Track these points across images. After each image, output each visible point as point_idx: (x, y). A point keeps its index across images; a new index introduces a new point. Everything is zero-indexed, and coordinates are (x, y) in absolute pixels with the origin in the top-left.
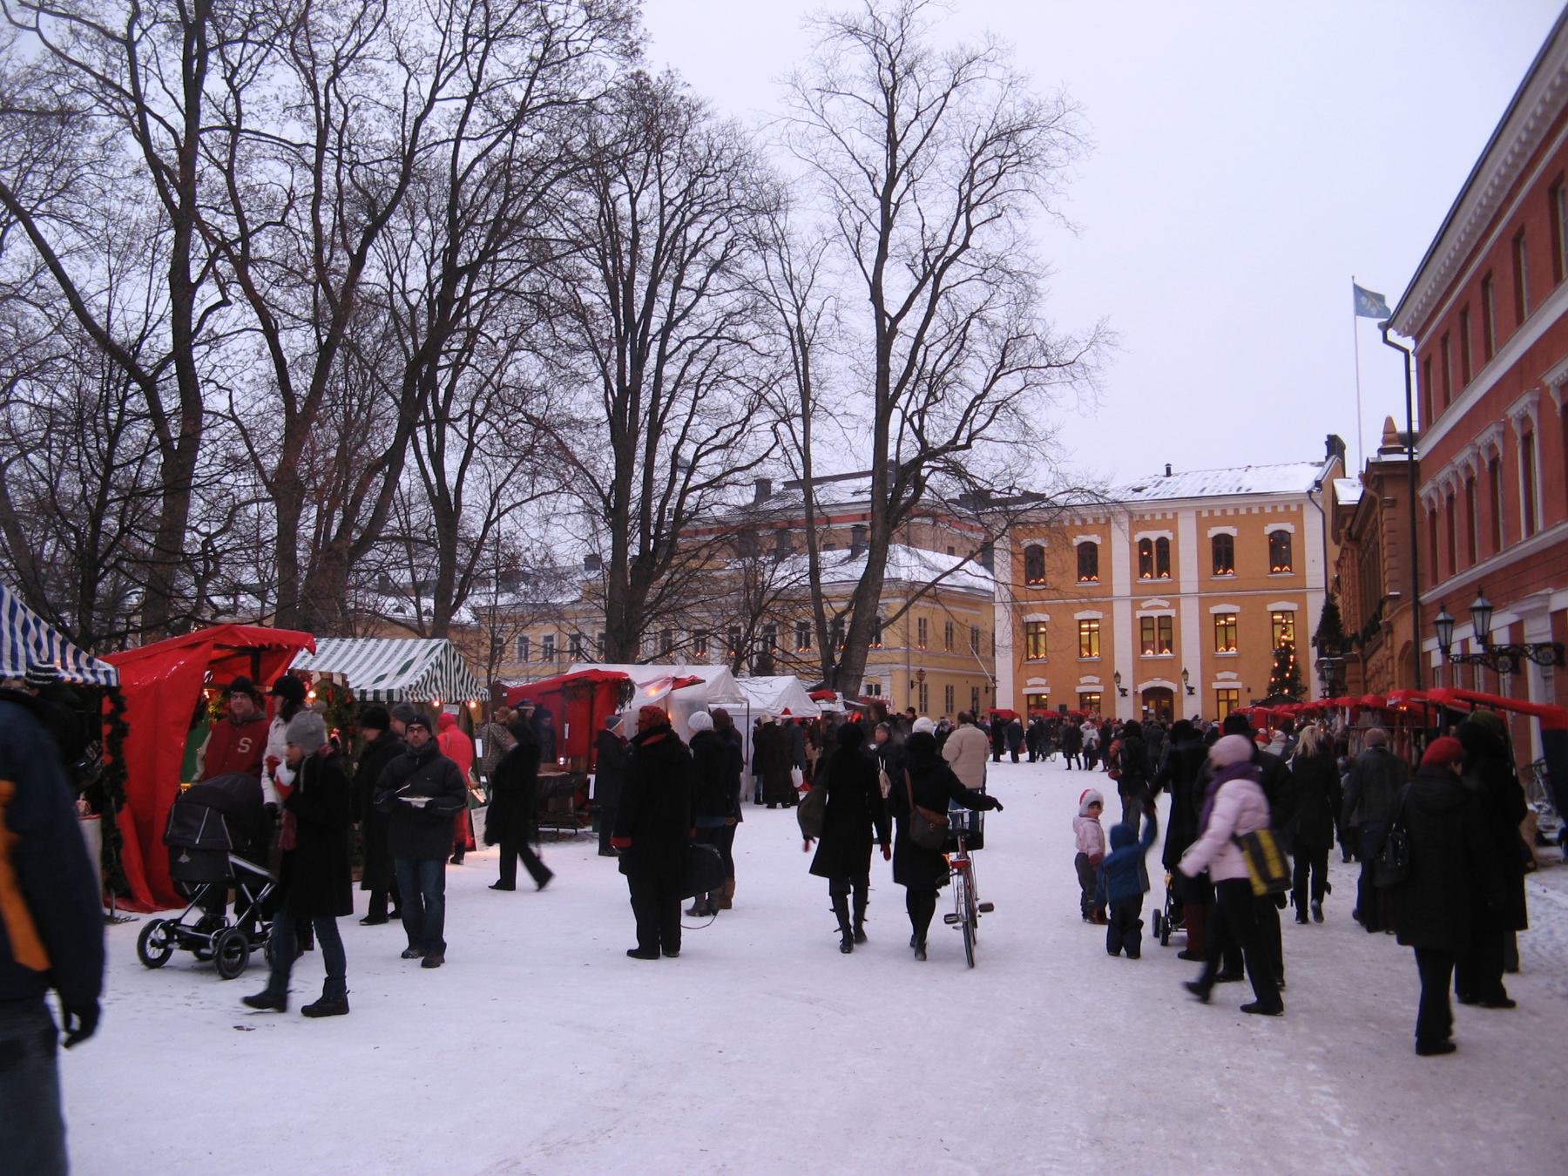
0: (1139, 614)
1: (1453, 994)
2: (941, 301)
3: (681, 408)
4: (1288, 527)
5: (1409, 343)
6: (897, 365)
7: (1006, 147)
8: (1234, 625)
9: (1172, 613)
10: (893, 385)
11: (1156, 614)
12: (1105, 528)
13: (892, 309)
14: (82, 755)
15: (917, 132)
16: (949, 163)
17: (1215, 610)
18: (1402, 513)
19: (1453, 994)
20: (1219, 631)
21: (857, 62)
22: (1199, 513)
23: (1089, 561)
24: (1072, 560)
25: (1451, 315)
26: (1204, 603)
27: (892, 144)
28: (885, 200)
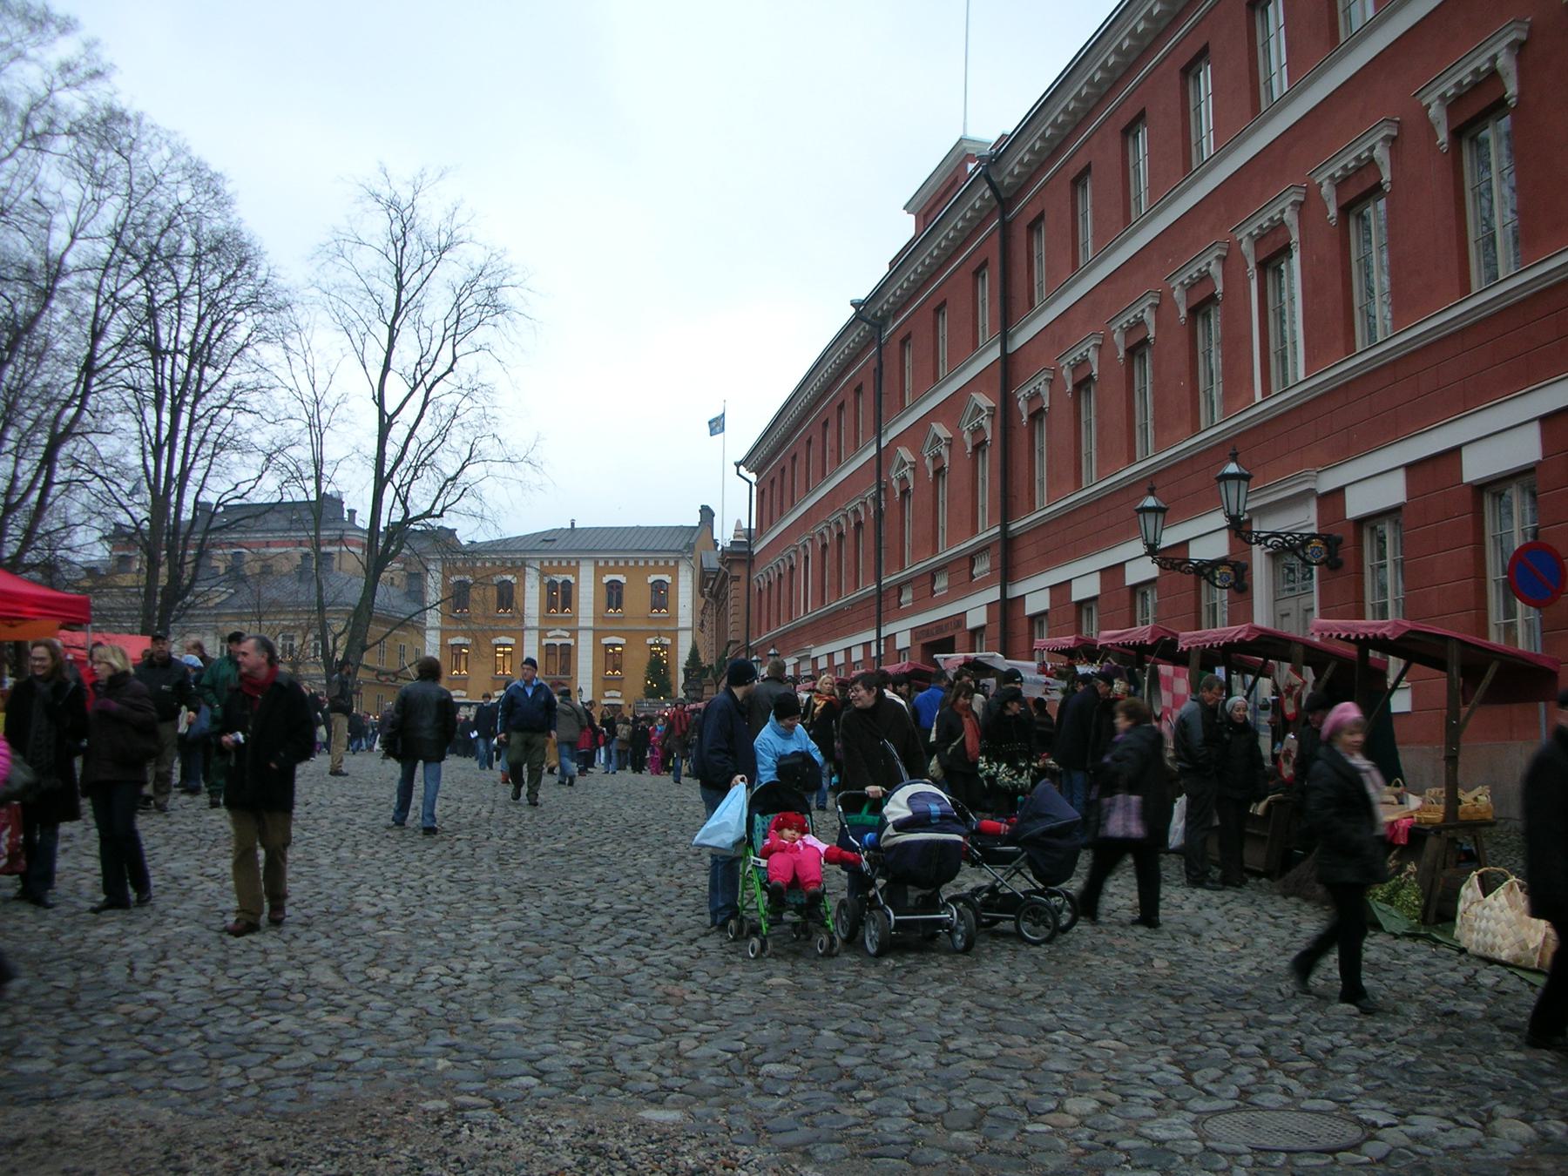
0: (545, 642)
1: (818, 756)
2: (430, 407)
3: (201, 463)
4: (668, 579)
5: (753, 477)
6: (392, 451)
7: (483, 300)
8: (620, 653)
9: (572, 642)
10: (387, 470)
11: (558, 642)
12: (519, 569)
13: (390, 409)
14: (1112, 794)
15: (418, 278)
16: (418, 282)
17: (605, 641)
18: (743, 584)
19: (818, 756)
20: (610, 659)
21: (378, 226)
22: (596, 563)
23: (508, 597)
24: (492, 593)
25: (780, 459)
26: (598, 634)
27: (400, 287)
28: (392, 327)
